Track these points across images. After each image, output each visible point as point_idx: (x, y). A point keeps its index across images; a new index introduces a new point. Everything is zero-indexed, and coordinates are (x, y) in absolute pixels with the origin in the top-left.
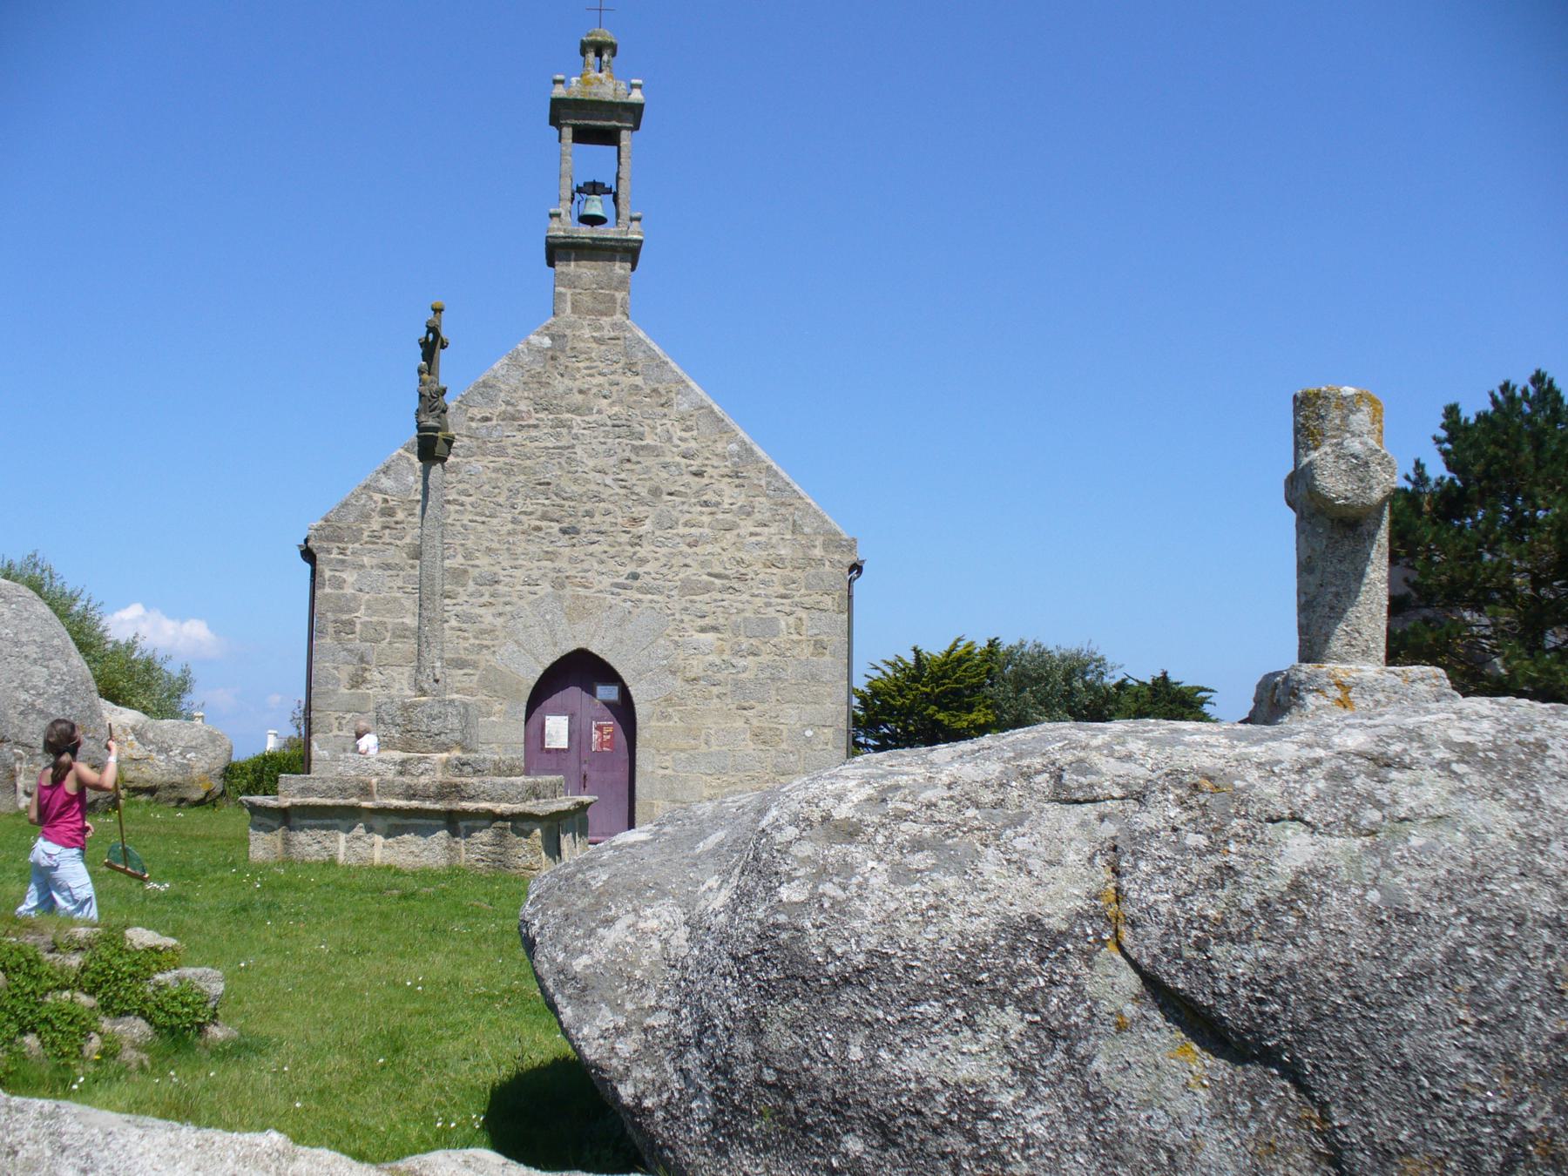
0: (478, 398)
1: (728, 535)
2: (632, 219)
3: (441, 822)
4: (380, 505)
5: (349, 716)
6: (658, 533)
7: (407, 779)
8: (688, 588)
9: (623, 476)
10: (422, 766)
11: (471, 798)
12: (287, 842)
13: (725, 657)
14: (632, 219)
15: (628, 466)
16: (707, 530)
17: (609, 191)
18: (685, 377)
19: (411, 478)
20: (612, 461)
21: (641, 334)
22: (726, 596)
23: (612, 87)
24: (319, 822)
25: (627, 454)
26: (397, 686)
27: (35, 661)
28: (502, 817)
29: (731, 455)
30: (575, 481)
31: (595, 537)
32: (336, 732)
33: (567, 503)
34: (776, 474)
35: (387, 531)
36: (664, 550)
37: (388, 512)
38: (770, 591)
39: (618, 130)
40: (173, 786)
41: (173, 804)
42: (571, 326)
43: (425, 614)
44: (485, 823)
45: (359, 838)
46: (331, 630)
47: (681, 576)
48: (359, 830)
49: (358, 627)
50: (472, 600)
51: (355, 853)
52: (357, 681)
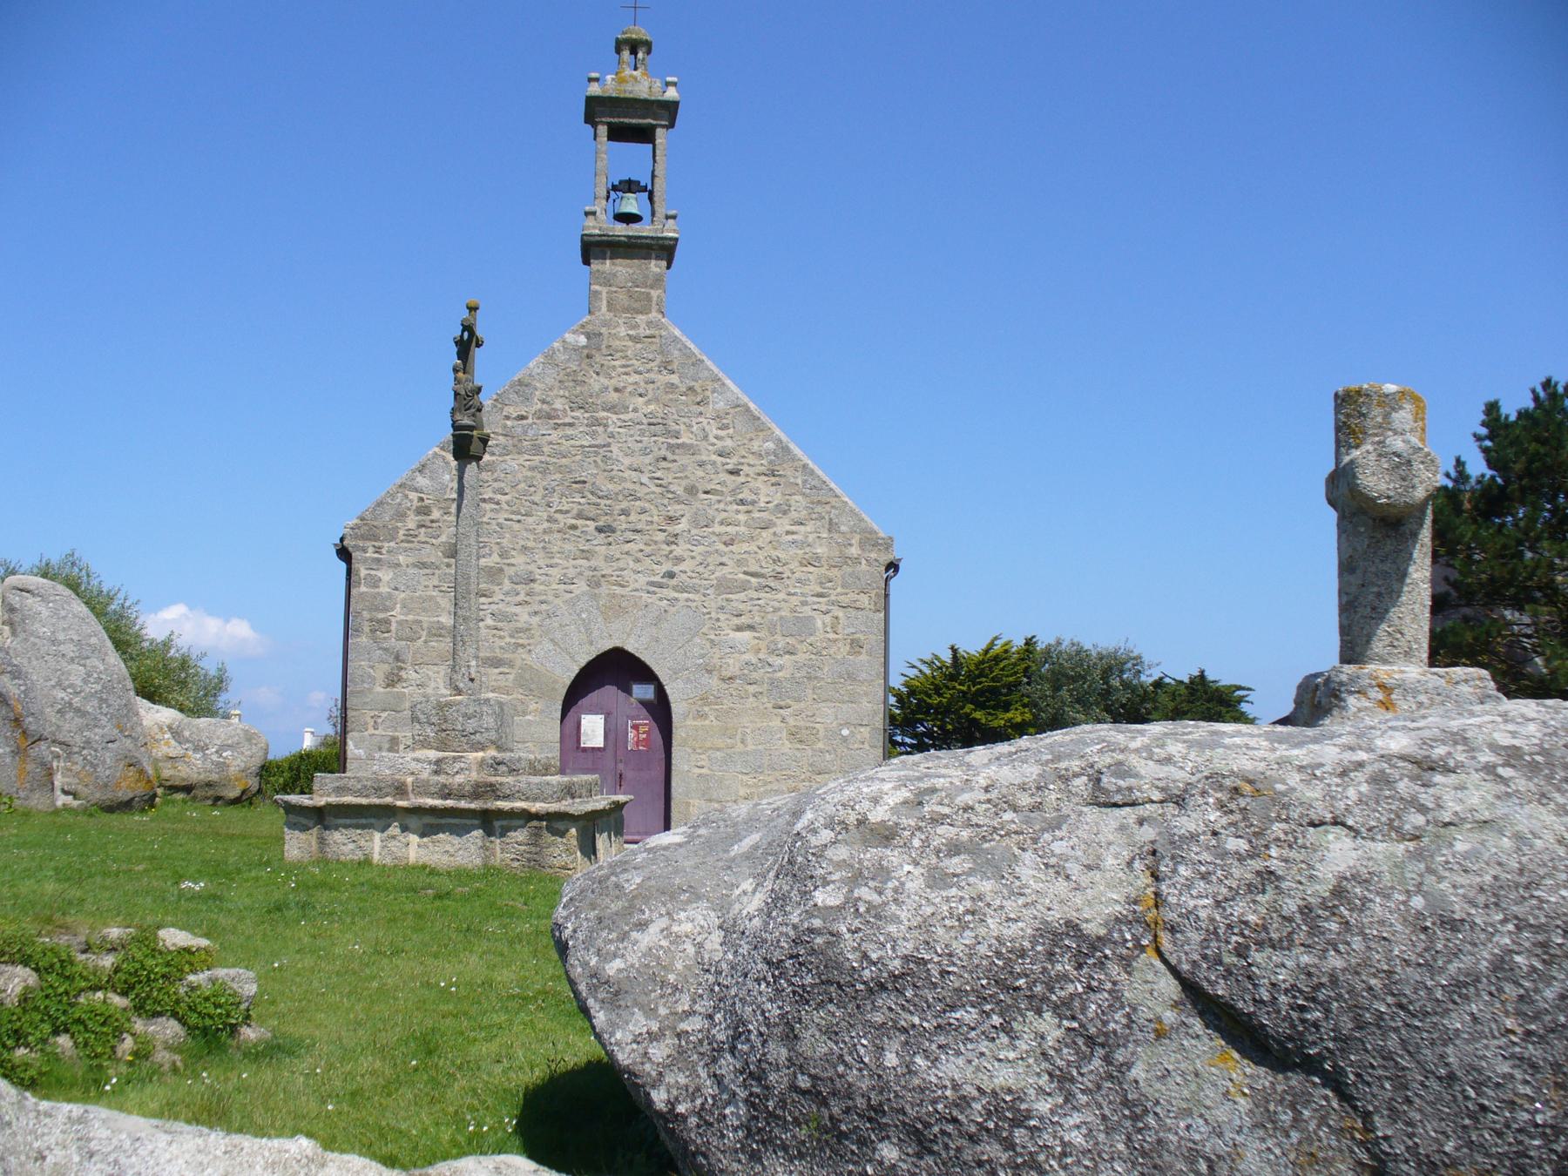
0: (513, 396)
1: (764, 534)
2: (668, 217)
3: (476, 822)
4: (416, 503)
5: (384, 715)
6: (694, 532)
7: (442, 779)
8: (725, 586)
9: (658, 474)
10: (457, 766)
11: (506, 797)
12: (322, 841)
13: (761, 656)
14: (668, 217)
15: (664, 464)
16: (742, 529)
17: (644, 189)
18: (721, 375)
19: (447, 477)
20: (648, 459)
21: (677, 332)
22: (762, 595)
23: (647, 84)
24: (354, 821)
25: (663, 452)
26: (433, 685)
27: (72, 659)
28: (537, 816)
29: (768, 454)
30: (611, 479)
31: (631, 536)
32: (371, 731)
33: (603, 502)
34: (812, 472)
35: (423, 530)
36: (701, 549)
37: (424, 511)
38: (806, 590)
39: (653, 128)
40: (209, 785)
41: (210, 802)
42: (606, 324)
43: (460, 612)
44: (521, 822)
45: (394, 837)
46: (367, 629)
47: (717, 574)
48: (394, 830)
49: (394, 627)
50: (508, 599)
51: (391, 853)
52: (393, 680)
